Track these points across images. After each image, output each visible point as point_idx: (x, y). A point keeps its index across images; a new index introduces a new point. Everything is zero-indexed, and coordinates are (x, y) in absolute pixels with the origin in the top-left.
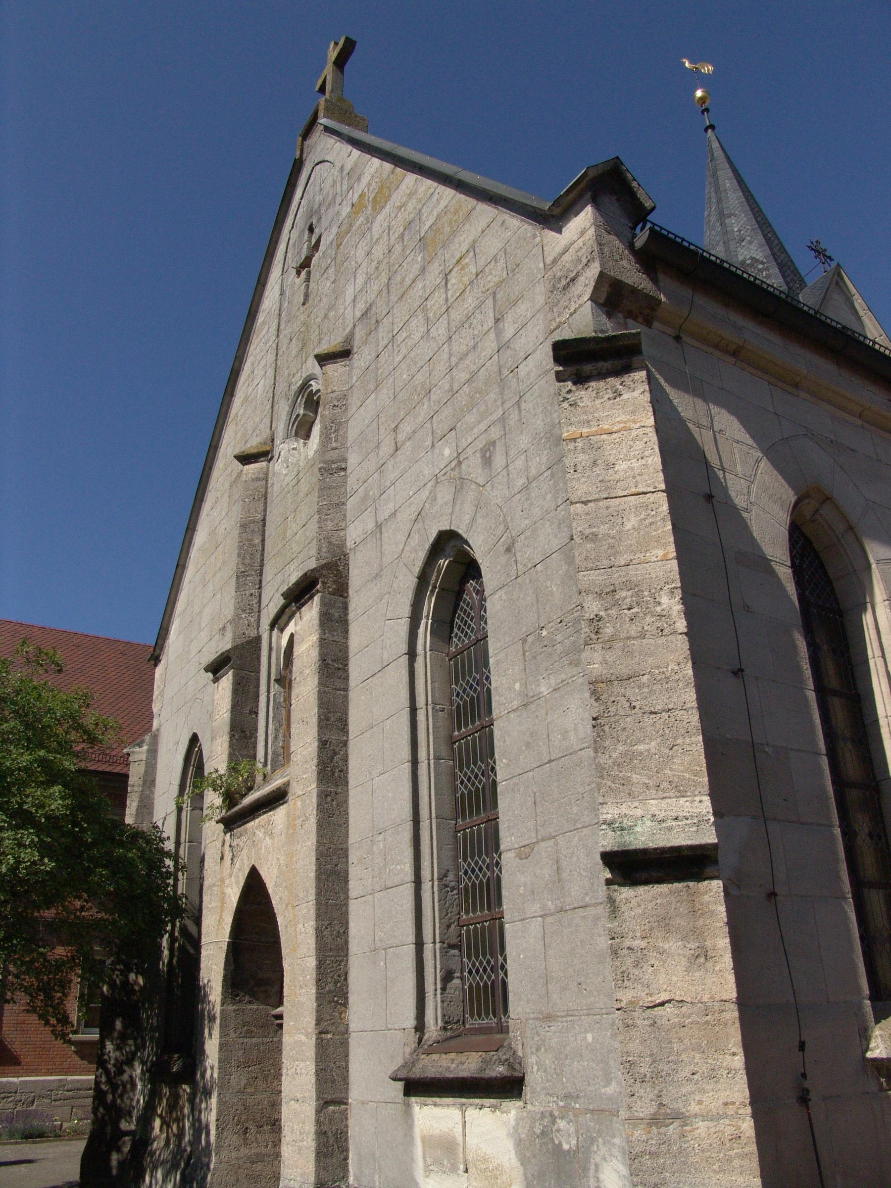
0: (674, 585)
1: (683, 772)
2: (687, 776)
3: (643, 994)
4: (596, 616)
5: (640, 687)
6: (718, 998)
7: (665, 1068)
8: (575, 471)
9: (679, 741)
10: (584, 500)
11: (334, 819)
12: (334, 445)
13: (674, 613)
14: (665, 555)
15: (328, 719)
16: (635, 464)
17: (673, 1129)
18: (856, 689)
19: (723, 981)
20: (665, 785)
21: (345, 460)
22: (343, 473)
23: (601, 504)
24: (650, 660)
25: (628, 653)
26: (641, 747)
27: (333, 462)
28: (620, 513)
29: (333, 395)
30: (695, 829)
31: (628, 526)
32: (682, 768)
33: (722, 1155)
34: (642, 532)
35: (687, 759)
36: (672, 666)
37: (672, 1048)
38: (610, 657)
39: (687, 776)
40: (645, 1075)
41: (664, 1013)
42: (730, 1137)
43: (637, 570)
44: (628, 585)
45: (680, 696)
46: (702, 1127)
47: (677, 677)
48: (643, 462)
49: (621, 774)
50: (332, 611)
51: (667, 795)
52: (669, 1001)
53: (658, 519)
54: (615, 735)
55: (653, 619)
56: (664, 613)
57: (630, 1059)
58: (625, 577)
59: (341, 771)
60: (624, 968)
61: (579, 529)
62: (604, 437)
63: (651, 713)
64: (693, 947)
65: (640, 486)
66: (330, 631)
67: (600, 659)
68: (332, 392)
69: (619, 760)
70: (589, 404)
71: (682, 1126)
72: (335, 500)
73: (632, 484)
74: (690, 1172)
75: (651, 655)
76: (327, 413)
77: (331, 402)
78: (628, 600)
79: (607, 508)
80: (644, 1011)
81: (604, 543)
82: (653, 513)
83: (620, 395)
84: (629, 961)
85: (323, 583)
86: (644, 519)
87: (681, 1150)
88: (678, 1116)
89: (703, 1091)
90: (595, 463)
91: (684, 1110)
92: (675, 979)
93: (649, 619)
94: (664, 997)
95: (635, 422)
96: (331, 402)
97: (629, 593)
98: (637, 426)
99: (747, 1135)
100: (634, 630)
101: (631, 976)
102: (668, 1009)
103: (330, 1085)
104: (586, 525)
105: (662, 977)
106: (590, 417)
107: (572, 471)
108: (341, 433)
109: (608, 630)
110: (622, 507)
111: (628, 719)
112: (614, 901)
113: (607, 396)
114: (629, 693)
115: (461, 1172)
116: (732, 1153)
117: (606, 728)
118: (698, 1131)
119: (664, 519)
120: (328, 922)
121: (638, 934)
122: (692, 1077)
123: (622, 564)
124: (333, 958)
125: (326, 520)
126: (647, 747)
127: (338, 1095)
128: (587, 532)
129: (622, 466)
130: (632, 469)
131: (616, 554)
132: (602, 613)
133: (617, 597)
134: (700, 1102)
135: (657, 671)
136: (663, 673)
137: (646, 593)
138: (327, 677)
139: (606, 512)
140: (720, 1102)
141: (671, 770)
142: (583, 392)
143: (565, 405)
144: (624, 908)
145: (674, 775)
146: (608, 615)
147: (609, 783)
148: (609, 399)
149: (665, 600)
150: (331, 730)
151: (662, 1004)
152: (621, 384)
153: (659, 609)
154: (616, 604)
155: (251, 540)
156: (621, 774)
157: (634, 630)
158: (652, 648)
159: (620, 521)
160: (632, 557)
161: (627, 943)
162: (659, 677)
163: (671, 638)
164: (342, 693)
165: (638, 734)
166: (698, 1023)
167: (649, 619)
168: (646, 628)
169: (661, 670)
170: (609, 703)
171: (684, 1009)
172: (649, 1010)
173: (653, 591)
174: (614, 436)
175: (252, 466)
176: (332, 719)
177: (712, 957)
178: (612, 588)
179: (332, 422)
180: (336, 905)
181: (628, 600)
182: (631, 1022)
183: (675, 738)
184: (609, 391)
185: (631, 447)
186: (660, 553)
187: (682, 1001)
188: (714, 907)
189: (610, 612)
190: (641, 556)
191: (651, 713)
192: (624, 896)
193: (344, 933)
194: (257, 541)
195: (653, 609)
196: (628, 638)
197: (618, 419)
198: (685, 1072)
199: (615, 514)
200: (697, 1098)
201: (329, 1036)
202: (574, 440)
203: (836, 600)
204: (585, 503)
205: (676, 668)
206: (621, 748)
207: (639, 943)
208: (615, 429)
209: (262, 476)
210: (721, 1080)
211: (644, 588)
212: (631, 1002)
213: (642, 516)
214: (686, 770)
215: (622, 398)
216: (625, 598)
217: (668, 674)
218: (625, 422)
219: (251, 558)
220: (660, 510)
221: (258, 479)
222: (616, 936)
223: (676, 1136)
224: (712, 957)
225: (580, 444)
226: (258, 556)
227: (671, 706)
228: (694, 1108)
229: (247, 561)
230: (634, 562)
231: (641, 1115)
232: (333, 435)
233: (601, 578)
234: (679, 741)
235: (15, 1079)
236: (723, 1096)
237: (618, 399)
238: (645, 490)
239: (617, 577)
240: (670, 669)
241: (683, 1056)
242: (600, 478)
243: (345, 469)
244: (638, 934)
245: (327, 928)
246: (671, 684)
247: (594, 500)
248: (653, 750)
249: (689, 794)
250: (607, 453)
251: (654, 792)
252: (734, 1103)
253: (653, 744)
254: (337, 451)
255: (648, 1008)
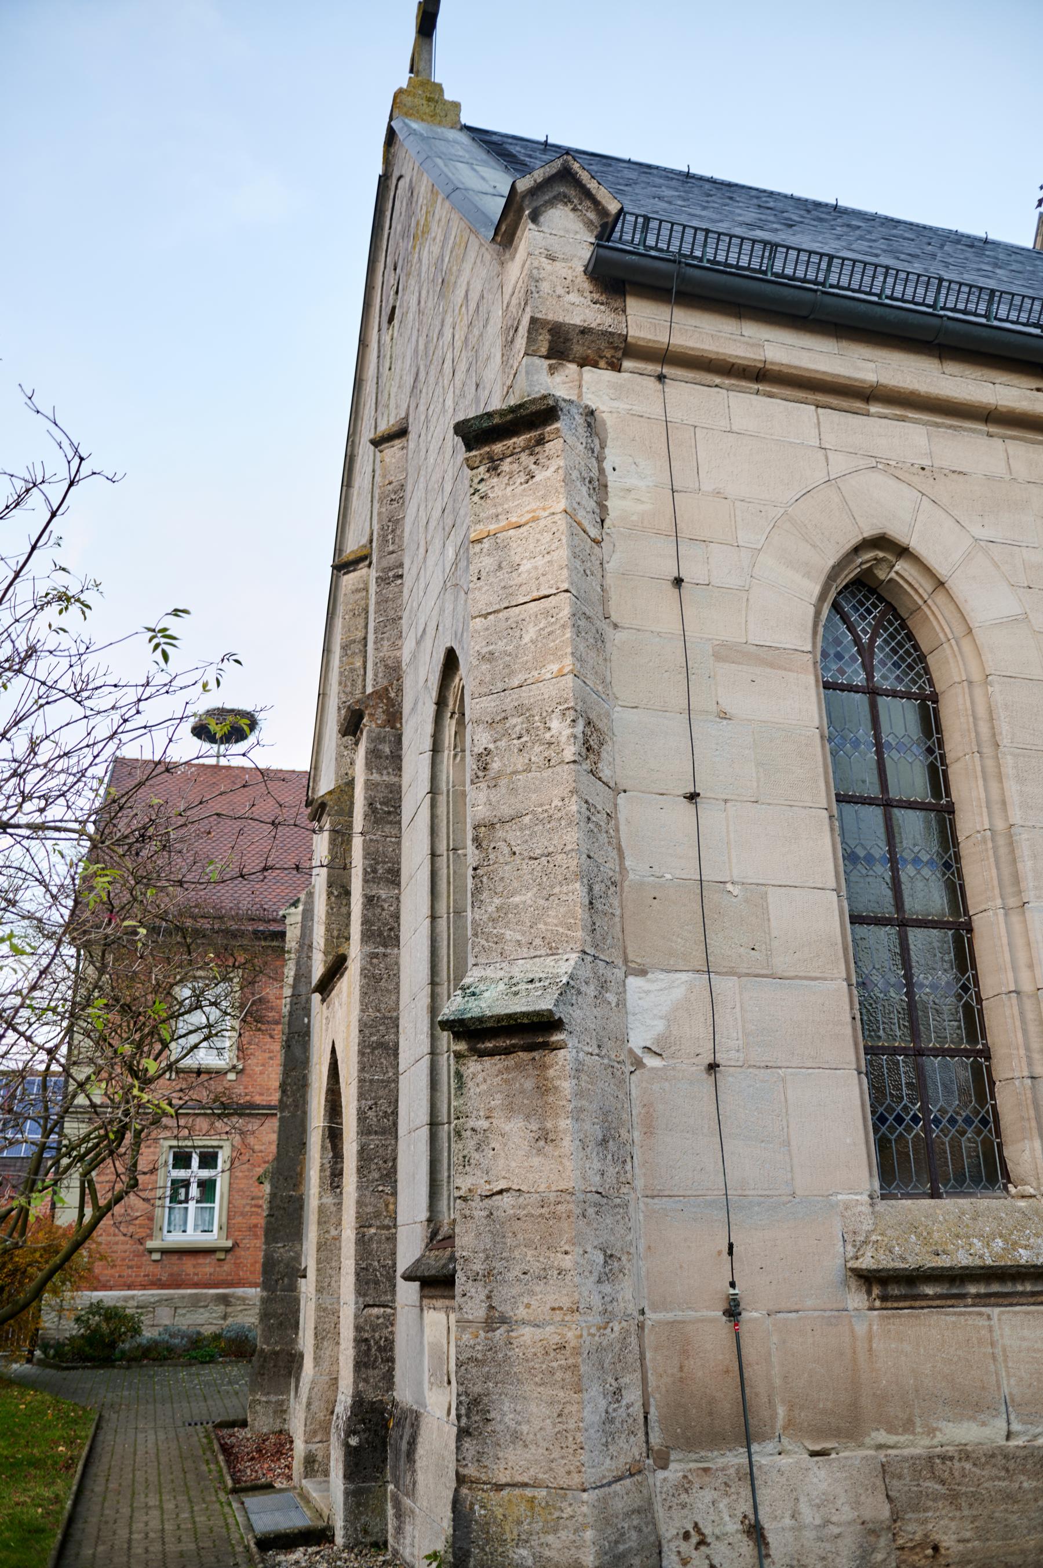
0: (566, 706)
1: (556, 926)
2: (561, 930)
3: (483, 1181)
4: (485, 749)
5: (521, 829)
6: (554, 1189)
7: (498, 1265)
8: (479, 579)
9: (556, 890)
10: (484, 612)
11: (383, 984)
12: (391, 548)
13: (563, 739)
14: (560, 670)
15: (375, 871)
16: (540, 562)
17: (500, 1332)
18: (948, 794)
19: (561, 1169)
20: (538, 941)
21: (401, 565)
22: (399, 582)
23: (501, 615)
24: (534, 796)
25: (513, 791)
26: (517, 899)
27: (390, 569)
28: (519, 625)
29: (390, 487)
30: (540, 993)
31: (526, 639)
32: (555, 921)
33: (544, 1366)
34: (540, 645)
35: (562, 910)
36: (557, 802)
37: (505, 1244)
38: (494, 796)
39: (561, 930)
40: (478, 1274)
41: (500, 1204)
42: (555, 1347)
43: (530, 690)
44: (520, 710)
45: (561, 837)
46: (526, 1334)
47: (560, 815)
48: (548, 558)
49: (495, 931)
50: (380, 747)
51: (538, 953)
52: (508, 1190)
53: (557, 626)
54: (492, 886)
55: (542, 748)
56: (553, 740)
57: (464, 1254)
58: (517, 700)
59: (391, 930)
60: (465, 1152)
61: (477, 648)
62: (512, 532)
63: (531, 858)
64: (534, 1129)
65: (542, 588)
66: (378, 769)
67: (485, 800)
68: (390, 483)
69: (495, 915)
70: (500, 493)
71: (508, 1332)
72: (392, 614)
73: (534, 588)
74: (512, 1384)
75: (535, 791)
76: (384, 510)
77: (388, 496)
78: (518, 728)
79: (507, 619)
80: (482, 1200)
81: (500, 662)
82: (553, 619)
83: (533, 477)
84: (471, 1144)
85: (371, 715)
86: (543, 629)
87: (506, 1358)
88: (504, 1320)
89: (532, 1293)
90: (500, 567)
91: (512, 1314)
92: (513, 1164)
93: (537, 749)
94: (502, 1185)
95: (544, 509)
96: (388, 496)
97: (520, 720)
98: (546, 514)
99: (572, 1345)
100: (520, 762)
101: (472, 1161)
102: (506, 1200)
103: (372, 1286)
104: (484, 643)
105: (501, 1162)
106: (500, 510)
107: (475, 579)
108: (398, 532)
109: (495, 765)
110: (522, 617)
111: (507, 868)
112: (462, 1076)
113: (519, 482)
114: (510, 837)
115: (446, 1384)
116: (555, 1364)
117: (485, 879)
118: (522, 1338)
119: (563, 626)
120: (373, 1102)
121: (482, 1114)
122: (522, 1277)
123: (516, 685)
124: (377, 1142)
125: (382, 639)
126: (523, 898)
127: (384, 1298)
128: (484, 651)
129: (526, 566)
130: (536, 568)
131: (512, 673)
132: (491, 746)
133: (507, 725)
134: (528, 1306)
135: (540, 810)
136: (546, 811)
137: (537, 718)
138: (374, 823)
139: (504, 625)
140: (548, 1307)
141: (546, 924)
142: (496, 480)
143: (476, 498)
144: (470, 1084)
145: (547, 930)
146: (497, 748)
147: (483, 942)
148: (521, 484)
149: (555, 724)
150: (379, 883)
151: (500, 1192)
152: (535, 463)
153: (548, 735)
154: (506, 733)
155: (352, 664)
156: (495, 931)
157: (520, 762)
158: (537, 783)
159: (518, 634)
160: (527, 676)
161: (471, 1123)
162: (542, 817)
163: (558, 769)
164: (393, 839)
165: (515, 884)
166: (532, 1216)
167: (537, 749)
168: (533, 759)
169: (545, 808)
170: (490, 850)
171: (521, 1199)
172: (487, 1201)
173: (544, 714)
174: (521, 530)
175: (352, 575)
176: (380, 871)
177: (552, 1141)
178: (503, 714)
179: (389, 521)
180: (382, 1081)
181: (518, 728)
182: (468, 1213)
183: (552, 887)
184: (522, 474)
185: (538, 541)
186: (555, 667)
187: (519, 1190)
188: (559, 1082)
189: (499, 743)
190: (535, 673)
191: (531, 858)
192: (471, 1070)
193: (392, 1113)
194: (359, 664)
195: (542, 736)
196: (514, 773)
197: (528, 508)
198: (516, 1272)
199: (514, 626)
200: (526, 1301)
201: (373, 1230)
202: (479, 541)
203: (931, 682)
204: (485, 616)
205: (560, 804)
206: (497, 901)
207: (483, 1124)
208: (523, 520)
209: (362, 586)
210: (551, 1282)
211: (535, 712)
212: (470, 1190)
213: (542, 625)
214: (561, 924)
215: (534, 480)
216: (515, 726)
217: (551, 812)
218: (534, 511)
219: (352, 685)
220: (561, 615)
221: (358, 591)
222: (460, 1115)
223: (501, 1343)
224: (552, 1141)
225: (486, 544)
226: (360, 681)
227: (550, 850)
228: (521, 1312)
229: (348, 689)
230: (529, 681)
231: (470, 1317)
232: (390, 537)
233: (493, 704)
234: (556, 890)
235: (705, 1314)
236: (551, 1300)
237: (530, 482)
238: (547, 593)
239: (510, 701)
240: (553, 805)
241: (516, 1253)
242: (502, 584)
243: (401, 576)
244: (482, 1114)
245: (371, 1108)
246: (553, 823)
247: (494, 612)
248: (529, 902)
249: (560, 951)
250: (513, 552)
251: (526, 950)
252: (561, 1308)
253: (529, 894)
254: (394, 555)
255: (487, 1196)
